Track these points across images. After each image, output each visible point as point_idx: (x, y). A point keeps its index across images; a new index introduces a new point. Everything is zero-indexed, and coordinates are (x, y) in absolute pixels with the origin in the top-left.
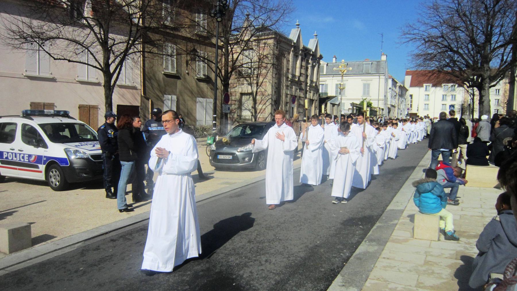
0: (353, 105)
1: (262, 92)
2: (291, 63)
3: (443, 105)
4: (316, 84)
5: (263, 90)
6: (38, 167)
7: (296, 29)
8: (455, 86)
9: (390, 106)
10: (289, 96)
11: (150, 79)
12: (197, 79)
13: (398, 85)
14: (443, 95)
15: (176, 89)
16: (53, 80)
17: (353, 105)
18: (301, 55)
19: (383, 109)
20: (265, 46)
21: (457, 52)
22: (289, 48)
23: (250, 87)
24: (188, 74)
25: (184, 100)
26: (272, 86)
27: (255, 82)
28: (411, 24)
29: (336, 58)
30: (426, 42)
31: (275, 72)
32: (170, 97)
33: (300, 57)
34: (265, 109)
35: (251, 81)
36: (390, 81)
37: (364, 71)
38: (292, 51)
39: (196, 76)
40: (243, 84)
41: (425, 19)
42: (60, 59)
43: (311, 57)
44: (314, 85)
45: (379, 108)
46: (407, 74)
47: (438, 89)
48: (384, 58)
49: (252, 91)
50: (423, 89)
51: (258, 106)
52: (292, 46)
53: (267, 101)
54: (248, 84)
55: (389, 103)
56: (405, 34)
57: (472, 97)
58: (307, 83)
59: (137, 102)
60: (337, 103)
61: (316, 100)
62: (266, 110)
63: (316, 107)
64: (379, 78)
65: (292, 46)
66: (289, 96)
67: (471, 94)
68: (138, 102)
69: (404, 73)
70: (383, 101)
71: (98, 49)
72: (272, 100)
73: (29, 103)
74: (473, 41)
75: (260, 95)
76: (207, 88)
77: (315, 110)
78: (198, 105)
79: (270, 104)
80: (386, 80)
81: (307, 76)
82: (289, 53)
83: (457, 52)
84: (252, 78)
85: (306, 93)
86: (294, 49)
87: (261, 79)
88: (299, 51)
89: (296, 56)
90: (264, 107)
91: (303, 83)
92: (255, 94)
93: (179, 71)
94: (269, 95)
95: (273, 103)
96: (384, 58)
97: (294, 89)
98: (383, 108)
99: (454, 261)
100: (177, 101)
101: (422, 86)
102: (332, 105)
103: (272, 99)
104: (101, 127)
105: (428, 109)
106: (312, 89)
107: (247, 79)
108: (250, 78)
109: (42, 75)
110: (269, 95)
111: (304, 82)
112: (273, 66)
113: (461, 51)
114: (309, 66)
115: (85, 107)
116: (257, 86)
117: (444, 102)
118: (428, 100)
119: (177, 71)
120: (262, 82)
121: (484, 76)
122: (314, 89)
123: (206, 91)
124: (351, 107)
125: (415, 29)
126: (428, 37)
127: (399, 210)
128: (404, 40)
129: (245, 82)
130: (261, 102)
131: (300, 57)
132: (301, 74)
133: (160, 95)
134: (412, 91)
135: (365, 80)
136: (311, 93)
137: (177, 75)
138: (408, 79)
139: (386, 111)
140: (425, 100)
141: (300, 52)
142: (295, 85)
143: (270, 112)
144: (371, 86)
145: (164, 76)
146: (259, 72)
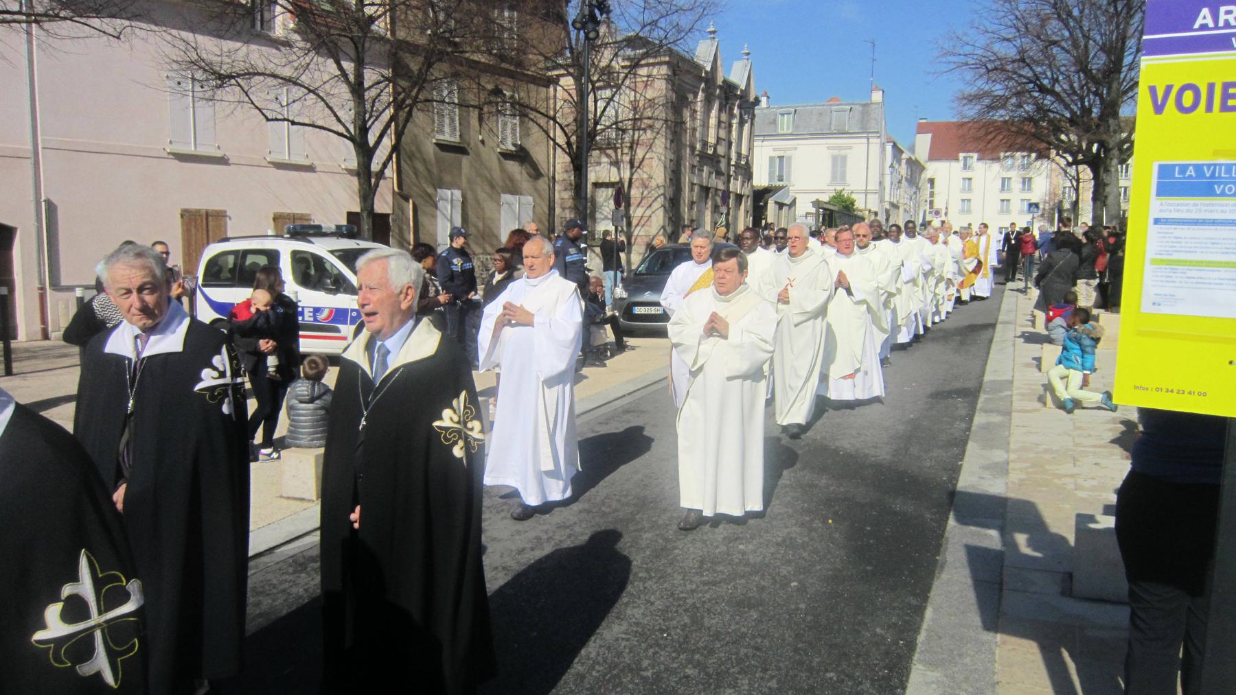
0: (817, 204)
1: (642, 179)
2: (699, 115)
3: (1003, 200)
4: (747, 160)
5: (645, 176)
6: (338, 331)
7: (709, 41)
8: (1029, 156)
10: (696, 188)
11: (410, 158)
12: (436, 144)
13: (904, 156)
14: (1003, 179)
15: (461, 175)
16: (223, 161)
17: (817, 204)
18: (719, 97)
19: (876, 214)
20: (647, 81)
21: (1052, 92)
23: (614, 169)
25: (477, 201)
26: (665, 167)
27: (627, 158)
29: (768, 97)
30: (989, 71)
31: (670, 136)
32: (449, 192)
33: (716, 106)
34: (650, 217)
35: (617, 156)
36: (889, 148)
37: (833, 128)
38: (703, 90)
39: (498, 146)
40: (599, 163)
41: (987, 24)
42: (277, 120)
43: (737, 102)
45: (870, 211)
46: (922, 129)
48: (877, 97)
49: (621, 179)
50: (956, 166)
51: (634, 212)
52: (701, 79)
53: (653, 201)
54: (611, 164)
55: (887, 198)
57: (1075, 184)
58: (729, 159)
59: (385, 206)
61: (748, 196)
62: (653, 218)
63: (748, 212)
65: (701, 79)
67: (1073, 178)
69: (914, 128)
70: (877, 195)
71: (342, 94)
72: (665, 198)
73: (179, 212)
74: (1082, 66)
77: (746, 217)
78: (504, 211)
79: (662, 206)
81: (730, 144)
83: (1052, 92)
84: (619, 151)
85: (729, 181)
86: (705, 85)
87: (640, 153)
89: (708, 102)
90: (648, 213)
91: (722, 160)
93: (466, 137)
94: (658, 187)
95: (667, 205)
96: (877, 97)
97: (705, 174)
98: (876, 210)
99: (1112, 426)
100: (463, 203)
101: (957, 159)
102: (777, 207)
104: (442, 253)
105: (969, 211)
106: (739, 171)
107: (609, 152)
108: (615, 149)
109: (202, 151)
110: (658, 187)
111: (724, 157)
112: (667, 125)
113: (1057, 88)
114: (735, 121)
115: (285, 218)
116: (632, 166)
117: (1005, 196)
118: (970, 189)
119: (460, 136)
120: (643, 159)
121: (1108, 144)
124: (813, 210)
125: (968, 44)
126: (993, 61)
127: (1005, 381)
128: (944, 67)
129: (604, 159)
131: (716, 106)
132: (719, 139)
133: (430, 190)
135: (833, 148)
136: (737, 180)
137: (462, 145)
138: (923, 143)
139: (882, 215)
140: (963, 190)
141: (718, 91)
143: (662, 224)
144: (849, 163)
145: (437, 149)
146: (636, 137)
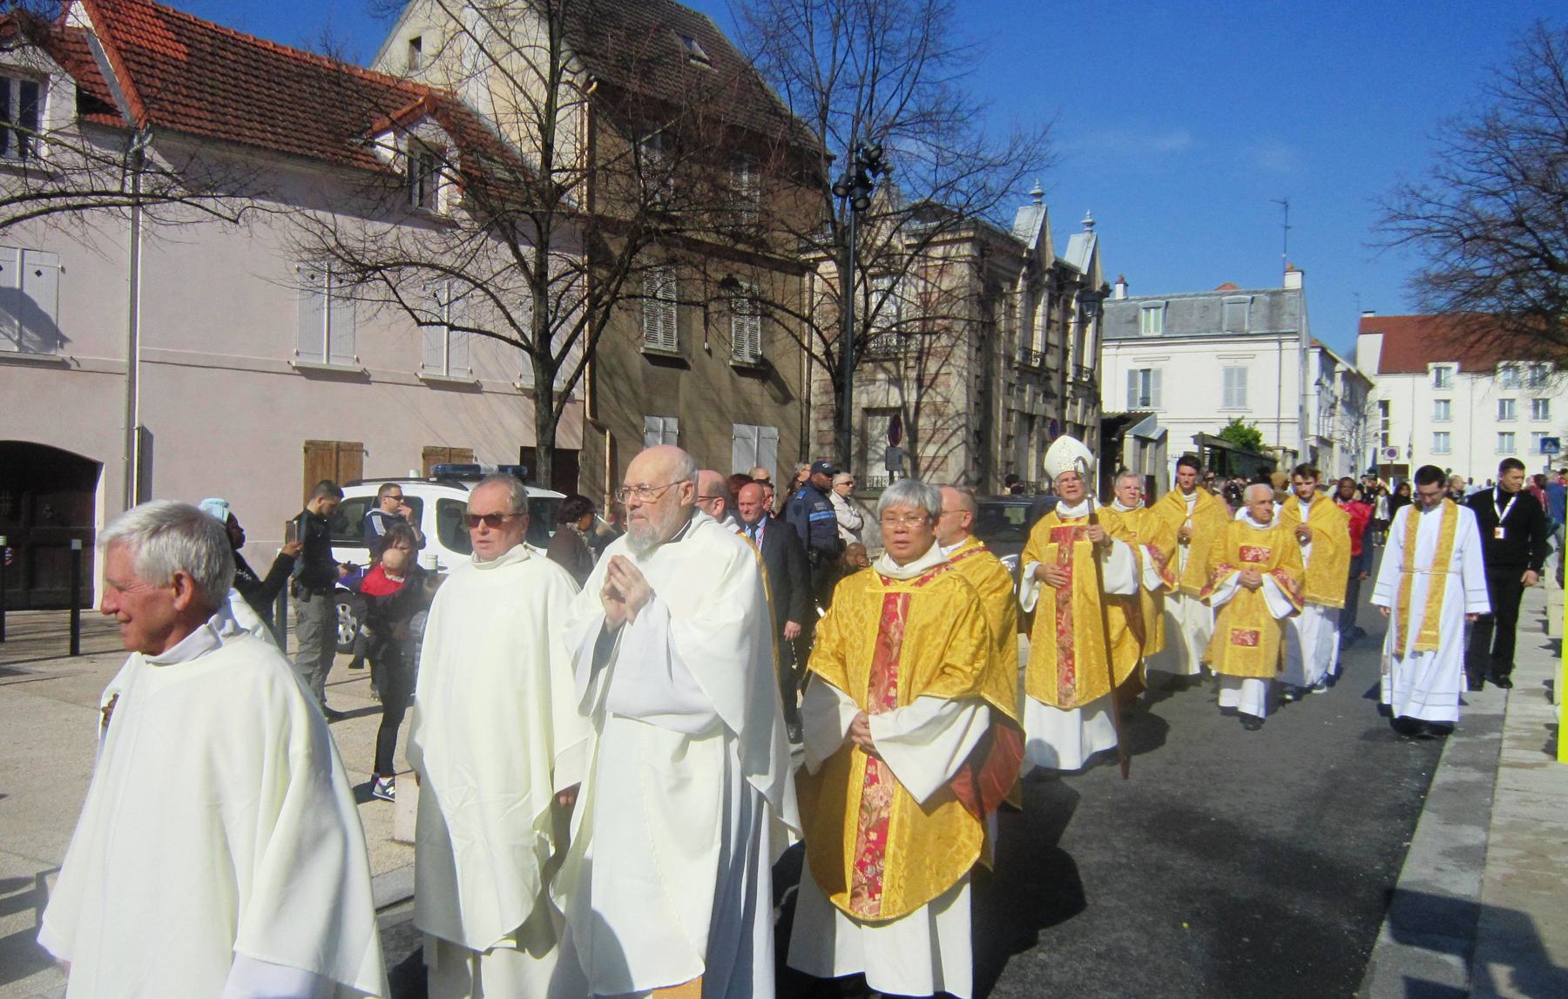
1: (934, 403)
5: (939, 399)
9: (1314, 444)
10: (1014, 417)
14: (1502, 402)
16: (362, 378)
18: (1050, 287)
22: (1013, 267)
23: (895, 392)
24: (709, 351)
26: (968, 387)
27: (913, 374)
28: (1415, 185)
29: (1126, 285)
31: (975, 343)
33: (1044, 300)
34: (946, 457)
35: (898, 370)
36: (1314, 356)
38: (1024, 277)
39: (731, 358)
40: (873, 381)
41: (1460, 170)
44: (1085, 379)
45: (1285, 450)
46: (1367, 327)
47: (1484, 382)
48: (1293, 281)
49: (904, 403)
50: (1424, 383)
51: (923, 450)
52: (1021, 261)
54: (890, 382)
55: (1313, 431)
56: (1393, 218)
58: (1065, 374)
60: (1154, 435)
62: (951, 460)
64: (1281, 350)
65: (1021, 261)
66: (1014, 417)
68: (576, 436)
69: (1355, 326)
72: (968, 429)
73: (303, 444)
75: (928, 416)
76: (762, 395)
80: (1304, 354)
81: (1065, 352)
82: (1014, 284)
84: (902, 363)
85: (1064, 406)
87: (932, 366)
88: (1042, 275)
90: (942, 452)
91: (1053, 375)
92: (912, 411)
95: (971, 440)
101: (1425, 372)
102: (1139, 443)
103: (966, 426)
106: (1079, 392)
107: (888, 365)
108: (896, 361)
111: (1056, 371)
116: (920, 386)
118: (1447, 417)
122: (1086, 392)
123: (759, 403)
125: (1429, 202)
128: (1391, 237)
130: (932, 436)
131: (1044, 300)
132: (1048, 345)
133: (635, 419)
134: (1386, 387)
135: (1228, 357)
138: (1370, 348)
141: (1047, 277)
142: (1031, 383)
144: (1251, 377)
145: (646, 361)
